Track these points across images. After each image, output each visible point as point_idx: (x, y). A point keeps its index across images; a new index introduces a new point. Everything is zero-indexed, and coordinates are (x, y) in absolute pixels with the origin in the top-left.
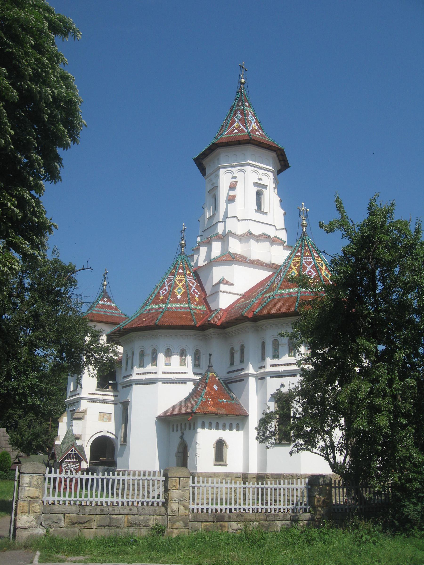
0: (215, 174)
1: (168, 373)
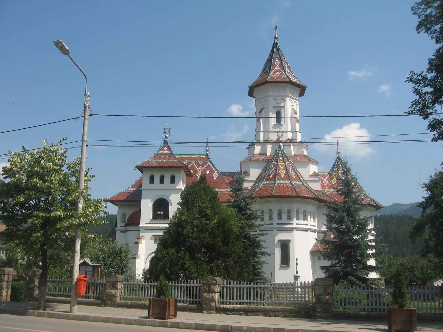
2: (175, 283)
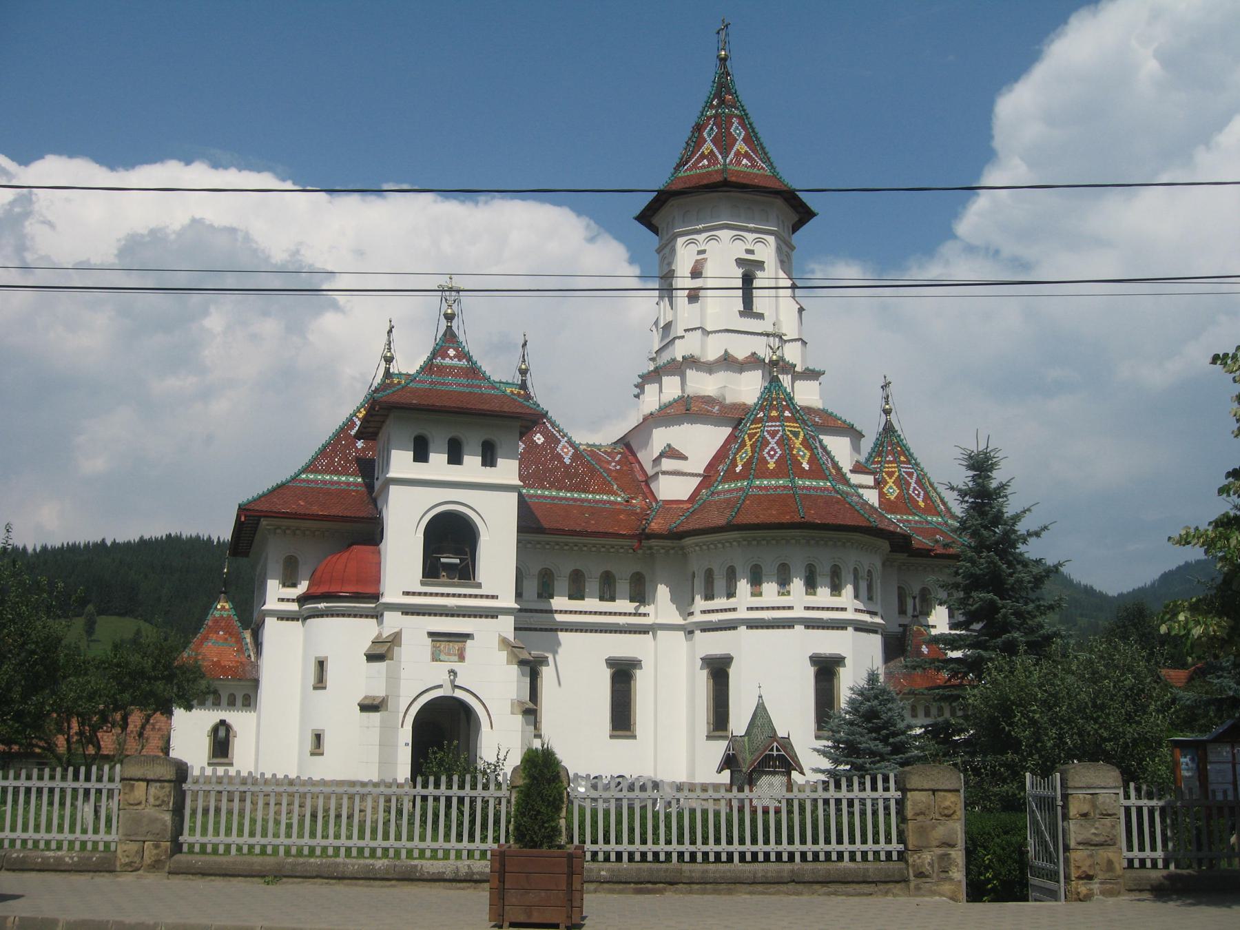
1: (757, 609)
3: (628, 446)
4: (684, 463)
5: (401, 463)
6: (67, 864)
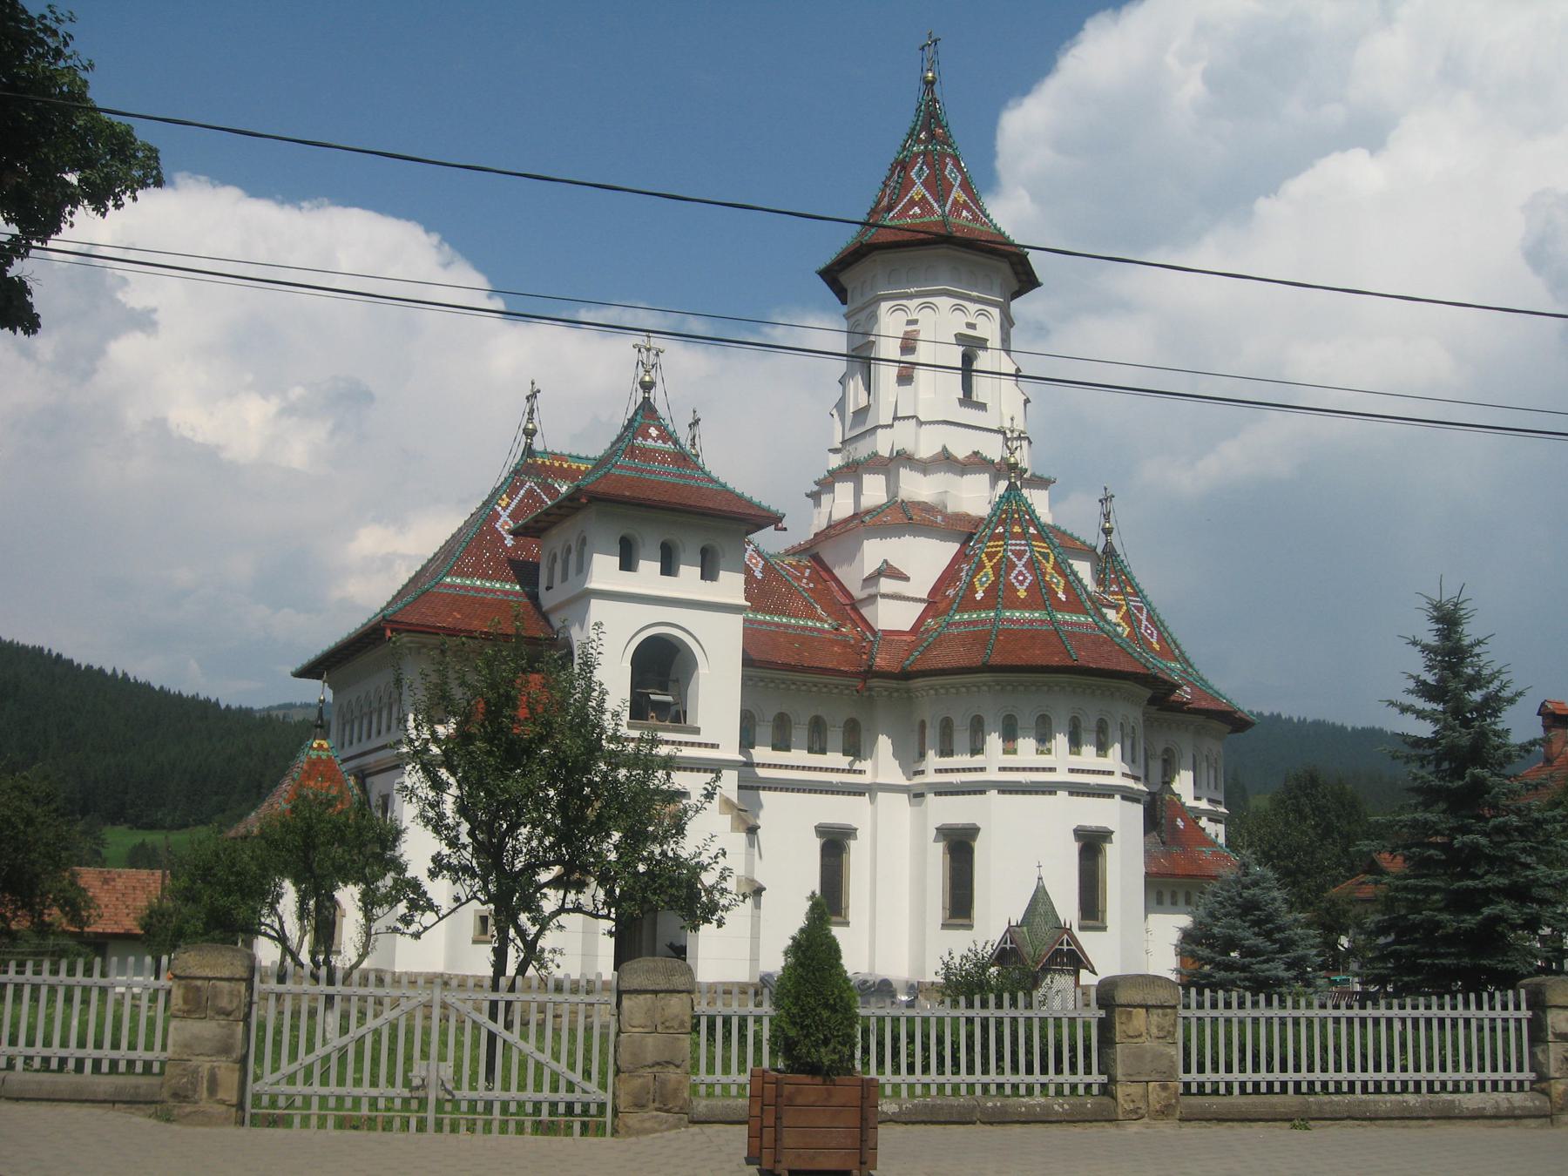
0: (868, 310)
1: (1011, 769)
2: (55, 972)
3: (817, 559)
4: (903, 582)
5: (604, 570)
6: (1057, 1113)
